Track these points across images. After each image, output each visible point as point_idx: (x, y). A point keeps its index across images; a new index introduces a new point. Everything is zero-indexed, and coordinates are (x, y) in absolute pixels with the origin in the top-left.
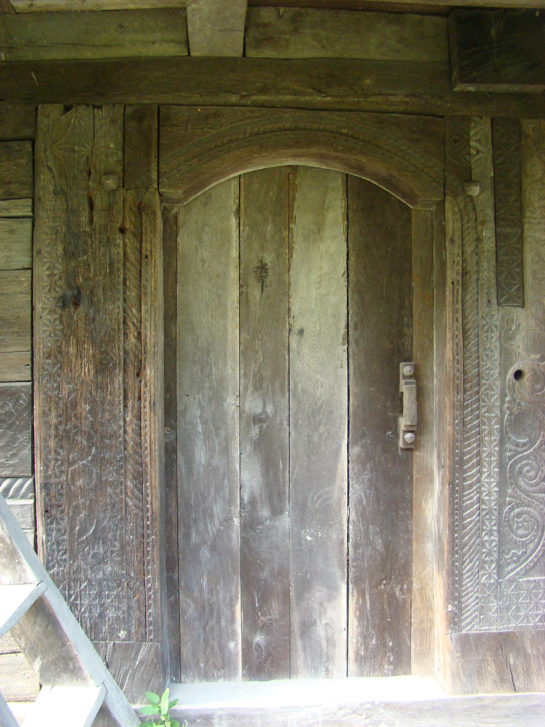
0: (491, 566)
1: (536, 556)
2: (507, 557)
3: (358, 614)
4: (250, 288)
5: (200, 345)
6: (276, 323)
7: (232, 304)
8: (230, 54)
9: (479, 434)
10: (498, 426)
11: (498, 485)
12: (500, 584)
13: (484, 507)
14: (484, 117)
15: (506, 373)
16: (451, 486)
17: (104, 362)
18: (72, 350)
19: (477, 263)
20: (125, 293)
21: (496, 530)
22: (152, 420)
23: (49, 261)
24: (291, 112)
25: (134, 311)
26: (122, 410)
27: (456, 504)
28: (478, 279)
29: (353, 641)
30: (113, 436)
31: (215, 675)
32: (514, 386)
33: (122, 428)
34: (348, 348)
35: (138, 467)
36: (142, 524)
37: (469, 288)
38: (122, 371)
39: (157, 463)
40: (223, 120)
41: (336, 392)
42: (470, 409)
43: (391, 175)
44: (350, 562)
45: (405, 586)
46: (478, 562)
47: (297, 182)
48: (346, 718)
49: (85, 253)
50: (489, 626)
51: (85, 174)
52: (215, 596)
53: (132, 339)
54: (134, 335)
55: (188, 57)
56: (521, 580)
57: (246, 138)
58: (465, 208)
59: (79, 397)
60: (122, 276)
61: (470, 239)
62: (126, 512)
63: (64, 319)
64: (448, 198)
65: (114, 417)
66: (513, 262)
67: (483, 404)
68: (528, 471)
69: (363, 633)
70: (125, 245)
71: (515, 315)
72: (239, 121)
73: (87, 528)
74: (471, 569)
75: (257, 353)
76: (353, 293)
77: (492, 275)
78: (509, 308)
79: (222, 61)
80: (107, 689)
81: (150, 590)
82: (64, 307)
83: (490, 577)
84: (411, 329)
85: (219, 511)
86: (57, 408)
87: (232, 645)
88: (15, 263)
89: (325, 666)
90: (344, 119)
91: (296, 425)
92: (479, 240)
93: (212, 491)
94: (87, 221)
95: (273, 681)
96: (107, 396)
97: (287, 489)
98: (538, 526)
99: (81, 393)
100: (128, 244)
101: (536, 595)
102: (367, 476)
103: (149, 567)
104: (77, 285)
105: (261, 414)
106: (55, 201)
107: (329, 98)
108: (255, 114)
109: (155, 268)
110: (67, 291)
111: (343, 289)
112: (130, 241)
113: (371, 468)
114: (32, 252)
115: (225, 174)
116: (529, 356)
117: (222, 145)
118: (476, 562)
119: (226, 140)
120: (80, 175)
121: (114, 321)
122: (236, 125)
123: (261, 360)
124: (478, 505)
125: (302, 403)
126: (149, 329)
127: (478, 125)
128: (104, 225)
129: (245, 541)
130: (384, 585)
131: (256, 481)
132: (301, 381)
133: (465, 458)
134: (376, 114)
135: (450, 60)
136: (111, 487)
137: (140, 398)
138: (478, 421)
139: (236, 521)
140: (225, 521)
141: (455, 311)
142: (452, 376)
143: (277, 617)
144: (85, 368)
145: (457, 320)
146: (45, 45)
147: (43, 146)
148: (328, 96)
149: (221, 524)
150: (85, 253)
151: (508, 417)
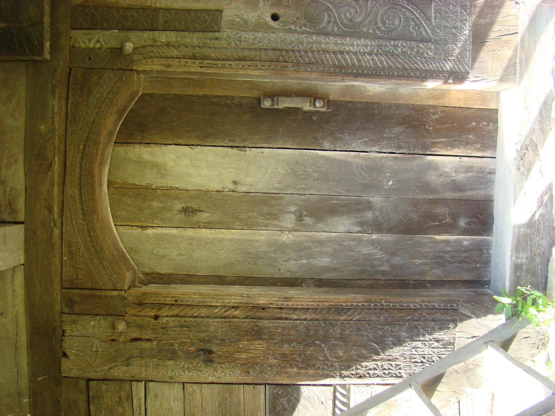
0: (421, 47)
1: (416, 11)
2: (415, 34)
3: (449, 148)
4: (201, 220)
5: (242, 259)
6: (228, 202)
7: (212, 234)
8: (22, 234)
9: (319, 52)
10: (314, 36)
11: (359, 38)
12: (435, 41)
13: (375, 51)
14: (71, 35)
15: (272, 28)
16: (358, 76)
17: (253, 333)
18: (243, 356)
19: (187, 47)
20: (203, 317)
21: (394, 42)
22: (298, 300)
23: (179, 371)
24: (67, 189)
25: (217, 310)
26: (289, 321)
27: (372, 72)
28: (199, 47)
29: (470, 153)
30: (307, 328)
31: (486, 256)
32: (283, 22)
33: (303, 322)
34: (248, 147)
35: (331, 311)
36: (372, 310)
37: (206, 55)
38: (261, 320)
39: (329, 297)
40: (74, 241)
41: (281, 157)
42: (300, 58)
43: (116, 112)
44: (411, 152)
45: (432, 110)
46: (418, 58)
47: (120, 182)
48: (526, 165)
49: (172, 345)
50: (467, 51)
51: (114, 343)
52: (428, 254)
53: (237, 313)
54: (234, 311)
55: (25, 265)
56: (433, 24)
57: (87, 224)
58: (142, 54)
59: (278, 352)
60: (191, 319)
61: (167, 52)
62: (364, 321)
63: (222, 361)
64: (134, 68)
65: (294, 327)
66: (186, 18)
67: (296, 47)
68: (350, 14)
69: (464, 145)
70: (167, 316)
71: (228, 18)
72: (74, 229)
73: (373, 349)
74: (422, 63)
75: (249, 216)
76: (206, 142)
77: (196, 35)
78: (222, 22)
79: (27, 240)
80: (490, 341)
81: (421, 306)
82: (212, 361)
83: (430, 49)
84: (236, 97)
85: (366, 249)
86: (285, 367)
87: (466, 243)
88: (179, 394)
89: (487, 175)
90: (72, 148)
91: (305, 189)
92: (168, 45)
93: (351, 253)
94: (148, 343)
95: (494, 214)
96: (278, 332)
97: (353, 198)
98: (393, 8)
99: (275, 350)
100: (166, 314)
101: (446, 13)
102: (346, 137)
103: (405, 305)
104: (196, 351)
105: (296, 215)
106: (134, 365)
107: (56, 159)
108: (69, 215)
109: (185, 295)
110: (200, 359)
111: (203, 150)
112: (164, 312)
113: (341, 133)
114: (171, 382)
115: (114, 238)
116: (260, 8)
117: (92, 242)
118: (417, 59)
119: (89, 239)
120: (115, 347)
121: (223, 326)
122: (77, 231)
123: (255, 214)
124: (373, 55)
125: (289, 184)
126: (230, 301)
127: (77, 41)
128: (152, 331)
129: (390, 231)
130: (429, 127)
131: (345, 221)
132: (272, 184)
133: (337, 64)
134: (68, 122)
135: (25, 61)
136: (345, 331)
137: (281, 308)
138: (309, 52)
139: (374, 237)
140: (374, 245)
141: (223, 66)
142: (274, 72)
143: (448, 209)
144: (257, 347)
145: (231, 65)
146: (17, 370)
147: (93, 373)
148: (54, 160)
149: (376, 248)
150: (172, 345)
151: (308, 28)
